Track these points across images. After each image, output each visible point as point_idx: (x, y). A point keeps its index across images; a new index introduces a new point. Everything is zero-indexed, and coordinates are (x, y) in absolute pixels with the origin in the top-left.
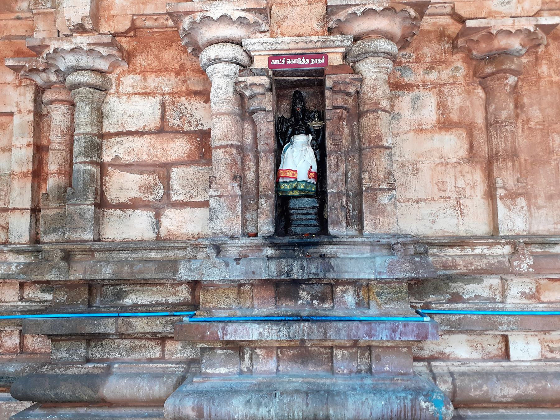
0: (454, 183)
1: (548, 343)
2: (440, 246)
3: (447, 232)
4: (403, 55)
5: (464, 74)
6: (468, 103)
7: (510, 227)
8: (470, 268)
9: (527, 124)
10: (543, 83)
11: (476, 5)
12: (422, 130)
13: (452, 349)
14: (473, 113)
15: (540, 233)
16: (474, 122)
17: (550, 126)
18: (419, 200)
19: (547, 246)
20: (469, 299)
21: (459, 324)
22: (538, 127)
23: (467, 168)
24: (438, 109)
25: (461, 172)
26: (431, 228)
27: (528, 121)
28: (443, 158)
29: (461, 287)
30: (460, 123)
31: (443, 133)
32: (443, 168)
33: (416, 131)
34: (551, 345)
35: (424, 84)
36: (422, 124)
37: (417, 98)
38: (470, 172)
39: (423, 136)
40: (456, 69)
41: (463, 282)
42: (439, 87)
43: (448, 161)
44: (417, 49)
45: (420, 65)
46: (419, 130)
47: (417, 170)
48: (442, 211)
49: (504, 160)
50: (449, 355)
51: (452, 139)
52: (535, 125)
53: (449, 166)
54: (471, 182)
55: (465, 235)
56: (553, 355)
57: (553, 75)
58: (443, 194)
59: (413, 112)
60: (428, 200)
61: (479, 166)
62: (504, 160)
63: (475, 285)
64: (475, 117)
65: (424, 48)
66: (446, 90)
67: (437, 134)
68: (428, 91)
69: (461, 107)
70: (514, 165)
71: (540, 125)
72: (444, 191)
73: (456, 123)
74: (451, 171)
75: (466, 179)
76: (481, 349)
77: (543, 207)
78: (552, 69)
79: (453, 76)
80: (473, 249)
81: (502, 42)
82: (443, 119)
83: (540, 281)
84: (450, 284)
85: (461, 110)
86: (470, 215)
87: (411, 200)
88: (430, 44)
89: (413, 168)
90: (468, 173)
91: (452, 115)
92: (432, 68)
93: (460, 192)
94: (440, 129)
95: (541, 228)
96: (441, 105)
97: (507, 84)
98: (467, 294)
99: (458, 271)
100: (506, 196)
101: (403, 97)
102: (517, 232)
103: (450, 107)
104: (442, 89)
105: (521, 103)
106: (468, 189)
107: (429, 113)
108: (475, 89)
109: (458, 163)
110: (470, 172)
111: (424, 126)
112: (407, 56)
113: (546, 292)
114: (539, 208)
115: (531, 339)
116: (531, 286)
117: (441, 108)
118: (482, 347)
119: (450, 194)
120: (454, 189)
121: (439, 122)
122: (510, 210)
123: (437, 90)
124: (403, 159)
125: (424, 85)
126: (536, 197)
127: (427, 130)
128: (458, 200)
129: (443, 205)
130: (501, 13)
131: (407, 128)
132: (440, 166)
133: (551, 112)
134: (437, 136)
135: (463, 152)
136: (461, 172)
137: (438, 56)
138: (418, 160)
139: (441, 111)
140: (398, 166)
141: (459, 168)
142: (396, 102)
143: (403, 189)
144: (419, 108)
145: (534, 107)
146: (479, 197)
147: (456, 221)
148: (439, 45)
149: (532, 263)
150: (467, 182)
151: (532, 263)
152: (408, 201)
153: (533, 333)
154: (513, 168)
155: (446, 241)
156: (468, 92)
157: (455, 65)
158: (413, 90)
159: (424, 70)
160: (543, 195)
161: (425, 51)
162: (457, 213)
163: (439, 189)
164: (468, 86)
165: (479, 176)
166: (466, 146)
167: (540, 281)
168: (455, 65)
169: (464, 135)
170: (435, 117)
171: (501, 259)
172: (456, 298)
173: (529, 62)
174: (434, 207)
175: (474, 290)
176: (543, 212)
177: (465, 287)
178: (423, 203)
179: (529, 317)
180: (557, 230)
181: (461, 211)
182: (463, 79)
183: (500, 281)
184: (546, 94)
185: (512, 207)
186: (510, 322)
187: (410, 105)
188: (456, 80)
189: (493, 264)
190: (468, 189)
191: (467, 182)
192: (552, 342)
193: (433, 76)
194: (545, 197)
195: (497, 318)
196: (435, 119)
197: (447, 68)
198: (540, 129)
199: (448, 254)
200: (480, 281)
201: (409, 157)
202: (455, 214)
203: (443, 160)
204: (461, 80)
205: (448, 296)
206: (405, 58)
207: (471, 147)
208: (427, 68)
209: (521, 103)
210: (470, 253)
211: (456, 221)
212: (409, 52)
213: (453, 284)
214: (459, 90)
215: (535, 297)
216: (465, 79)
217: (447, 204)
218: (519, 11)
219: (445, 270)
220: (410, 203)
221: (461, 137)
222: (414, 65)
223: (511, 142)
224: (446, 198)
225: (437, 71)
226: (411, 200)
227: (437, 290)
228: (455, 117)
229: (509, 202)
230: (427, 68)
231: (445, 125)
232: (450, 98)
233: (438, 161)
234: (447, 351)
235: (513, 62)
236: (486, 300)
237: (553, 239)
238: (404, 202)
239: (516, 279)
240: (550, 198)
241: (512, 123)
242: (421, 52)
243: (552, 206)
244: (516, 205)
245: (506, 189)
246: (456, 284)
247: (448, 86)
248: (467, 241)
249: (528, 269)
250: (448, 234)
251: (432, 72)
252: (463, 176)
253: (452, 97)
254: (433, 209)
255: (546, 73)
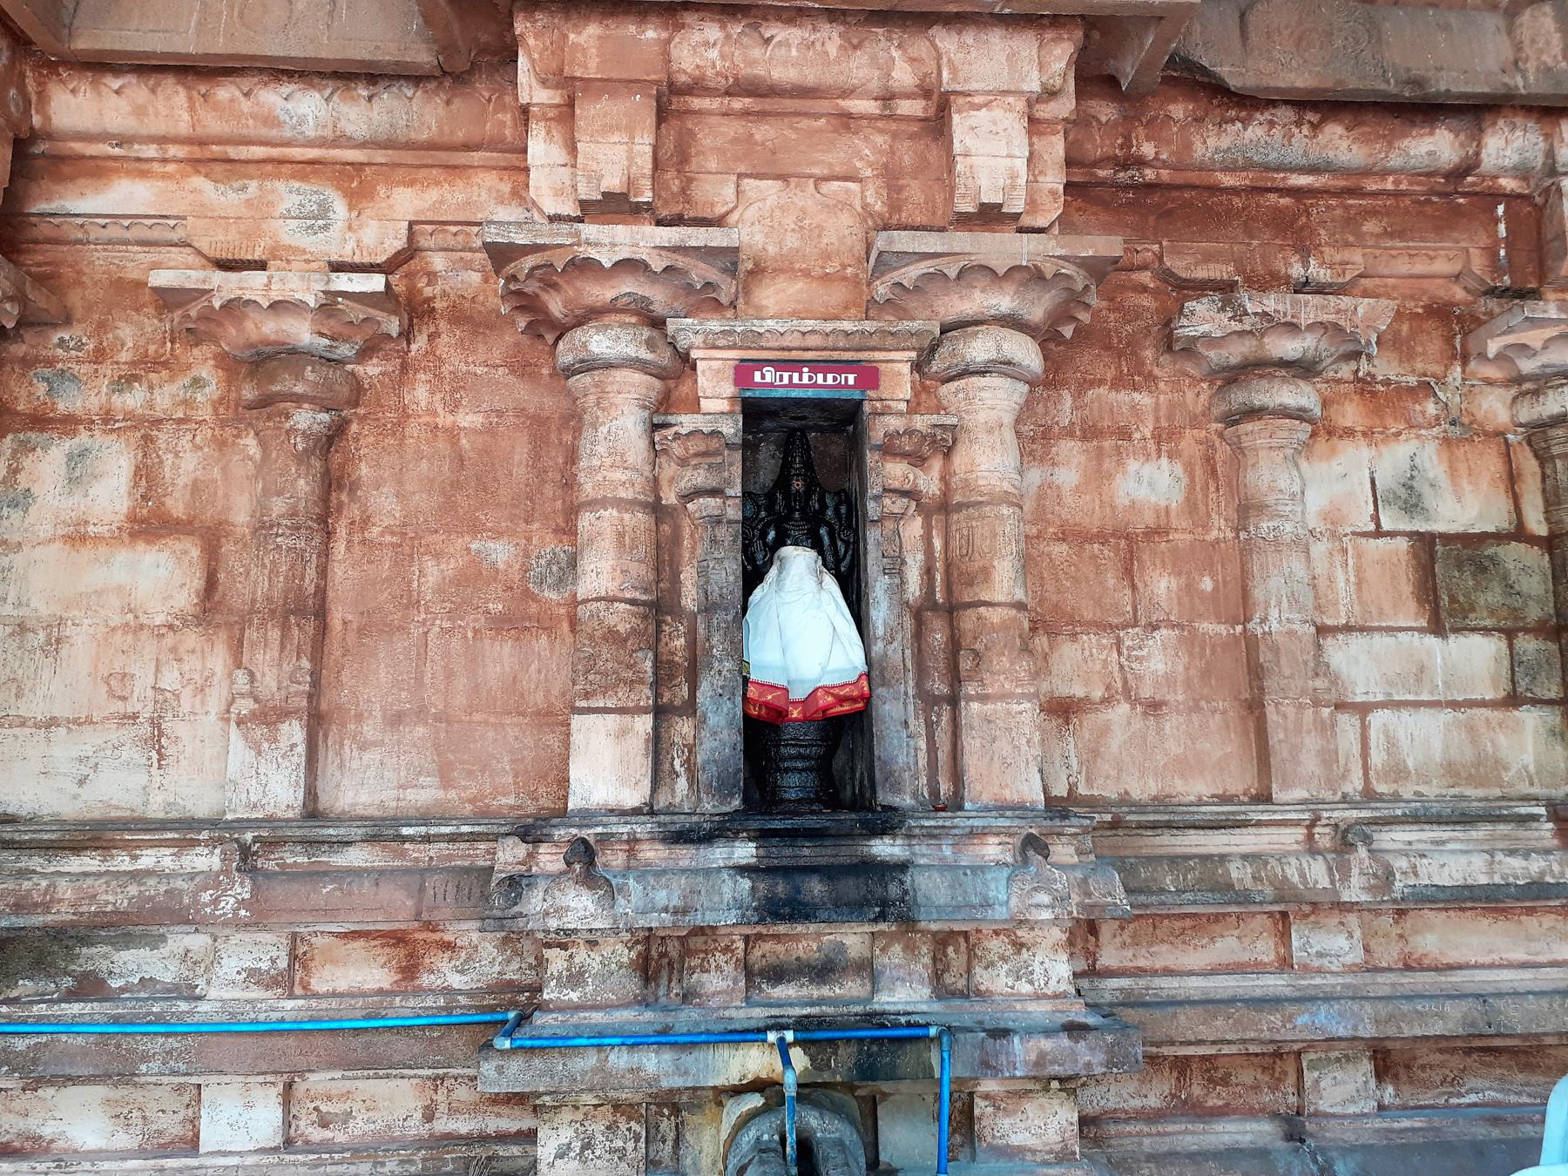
0: (152, 677)
1: (318, 1103)
2: (48, 849)
3: (117, 808)
4: (62, 340)
5: (215, 397)
6: (216, 472)
7: (253, 799)
8: (84, 909)
9: (363, 530)
10: (413, 428)
11: (242, 228)
12: (84, 538)
13: (61, 1126)
14: (227, 496)
15: (360, 811)
16: (227, 522)
17: (417, 537)
18: (51, 723)
19: (325, 847)
20: (123, 990)
21: (35, 1061)
22: (388, 538)
23: (192, 638)
24: (136, 485)
25: (173, 650)
26: (76, 797)
27: (366, 522)
28: (130, 611)
29: (105, 956)
30: (190, 523)
31: (141, 546)
32: (129, 637)
33: (70, 539)
34: (323, 1108)
35: (107, 417)
36: (86, 522)
37: (83, 453)
38: (198, 649)
39: (86, 553)
40: (197, 383)
41: (112, 944)
42: (145, 428)
43: (143, 620)
44: (102, 327)
45: (102, 368)
46: (77, 537)
47: (58, 641)
48: (109, 753)
49: (263, 624)
50: (52, 1141)
51: (162, 562)
52: (382, 534)
53: (145, 634)
54: (196, 677)
55: (161, 815)
56: (328, 1134)
57: (440, 411)
58: (119, 707)
59: (67, 490)
60: (76, 721)
61: (223, 635)
62: (263, 624)
63: (144, 953)
64: (230, 509)
65: (121, 324)
66: (162, 437)
67: (123, 550)
68: (114, 436)
69: (196, 481)
70: (284, 636)
71: (393, 534)
72: (124, 699)
73: (178, 522)
74: (149, 648)
75: (186, 667)
76: (140, 1121)
77: (375, 744)
78: (439, 396)
79: (185, 402)
80: (135, 858)
81: (270, 328)
82: (145, 512)
83: (314, 940)
84: (77, 950)
85: (196, 487)
86: (184, 763)
87: (30, 723)
88: (136, 317)
89: (49, 636)
90: (193, 651)
91: (169, 502)
92: (136, 378)
93: (164, 701)
94: (134, 535)
95: (364, 798)
96: (146, 476)
97: (292, 430)
98: (121, 976)
99: (49, 918)
100: (253, 716)
101: (45, 449)
102: (270, 810)
103: (168, 480)
104: (155, 433)
105: (354, 477)
106: (186, 693)
107: (111, 492)
108: (238, 436)
109: (171, 627)
110: (198, 649)
111: (91, 528)
112: (72, 344)
113: (328, 966)
114: (363, 747)
115: (257, 1093)
116: (274, 954)
117: (143, 483)
118: (144, 1118)
119: (138, 707)
120: (150, 693)
121: (132, 518)
122: (259, 753)
123: (139, 435)
124: (23, 612)
125: (105, 422)
126: (359, 718)
127: (97, 538)
128: (156, 723)
129: (114, 735)
130: (304, 252)
131: (45, 531)
132: (120, 632)
133: (424, 502)
134: (123, 556)
135: (185, 599)
136: (173, 650)
137: (152, 348)
138: (65, 615)
139: (142, 490)
140: (9, 630)
141: (170, 639)
142: (27, 462)
143: (14, 691)
144: (85, 479)
145: (385, 490)
146: (213, 717)
147: (143, 779)
148: (161, 320)
149: (247, 896)
150: (187, 677)
151: (247, 896)
152: (23, 724)
153: (261, 1079)
154: (282, 647)
155: (54, 837)
156: (221, 444)
157: (195, 372)
158: (74, 433)
159: (112, 383)
160: (378, 713)
161: (121, 333)
162: (150, 758)
163: (112, 694)
164: (222, 428)
165: (220, 661)
166: (198, 583)
167: (314, 940)
168: (195, 372)
169: (195, 553)
170: (123, 505)
171: (179, 884)
172: (90, 987)
173: (383, 374)
174: (89, 741)
175: (139, 966)
176: (372, 756)
177: (115, 958)
178: (62, 730)
179: (221, 1039)
180: (403, 804)
181: (159, 752)
182: (210, 410)
183: (210, 941)
184: (420, 456)
185: (266, 745)
186: (169, 1053)
187: (63, 471)
188: (193, 413)
189: (151, 898)
190: (186, 693)
191: (187, 677)
192: (329, 1098)
193: (134, 400)
194: (384, 717)
195: (137, 1042)
196: (125, 511)
197: (172, 379)
198: (393, 545)
199: (66, 869)
200: (156, 942)
201: (41, 606)
202: (144, 761)
203: (130, 617)
204: (206, 413)
205: (68, 982)
206: (68, 349)
207: (211, 584)
208: (120, 377)
209: (354, 477)
210: (123, 868)
211: (143, 779)
212: (79, 333)
213: (84, 950)
214: (198, 439)
215: (287, 980)
216: (215, 410)
217: (128, 733)
218: (347, 253)
219: (17, 915)
220: (27, 731)
221: (186, 559)
222: (86, 369)
223: (286, 577)
224: (125, 717)
225: (145, 386)
226: (30, 723)
227: (41, 965)
228: (177, 506)
229: (259, 732)
230: (120, 377)
231: (149, 524)
232: (170, 456)
233: (116, 620)
234: (47, 1131)
235: (299, 376)
236: (169, 991)
237: (331, 831)
238: (10, 726)
239: (239, 936)
240: (396, 720)
241: (298, 529)
242: (110, 336)
243: (399, 742)
244: (276, 741)
245: (256, 700)
246: (94, 950)
247: (168, 426)
248: (109, 835)
249: (235, 911)
250: (119, 814)
251: (131, 388)
252: (180, 660)
253: (177, 455)
254: (88, 747)
255: (423, 404)
